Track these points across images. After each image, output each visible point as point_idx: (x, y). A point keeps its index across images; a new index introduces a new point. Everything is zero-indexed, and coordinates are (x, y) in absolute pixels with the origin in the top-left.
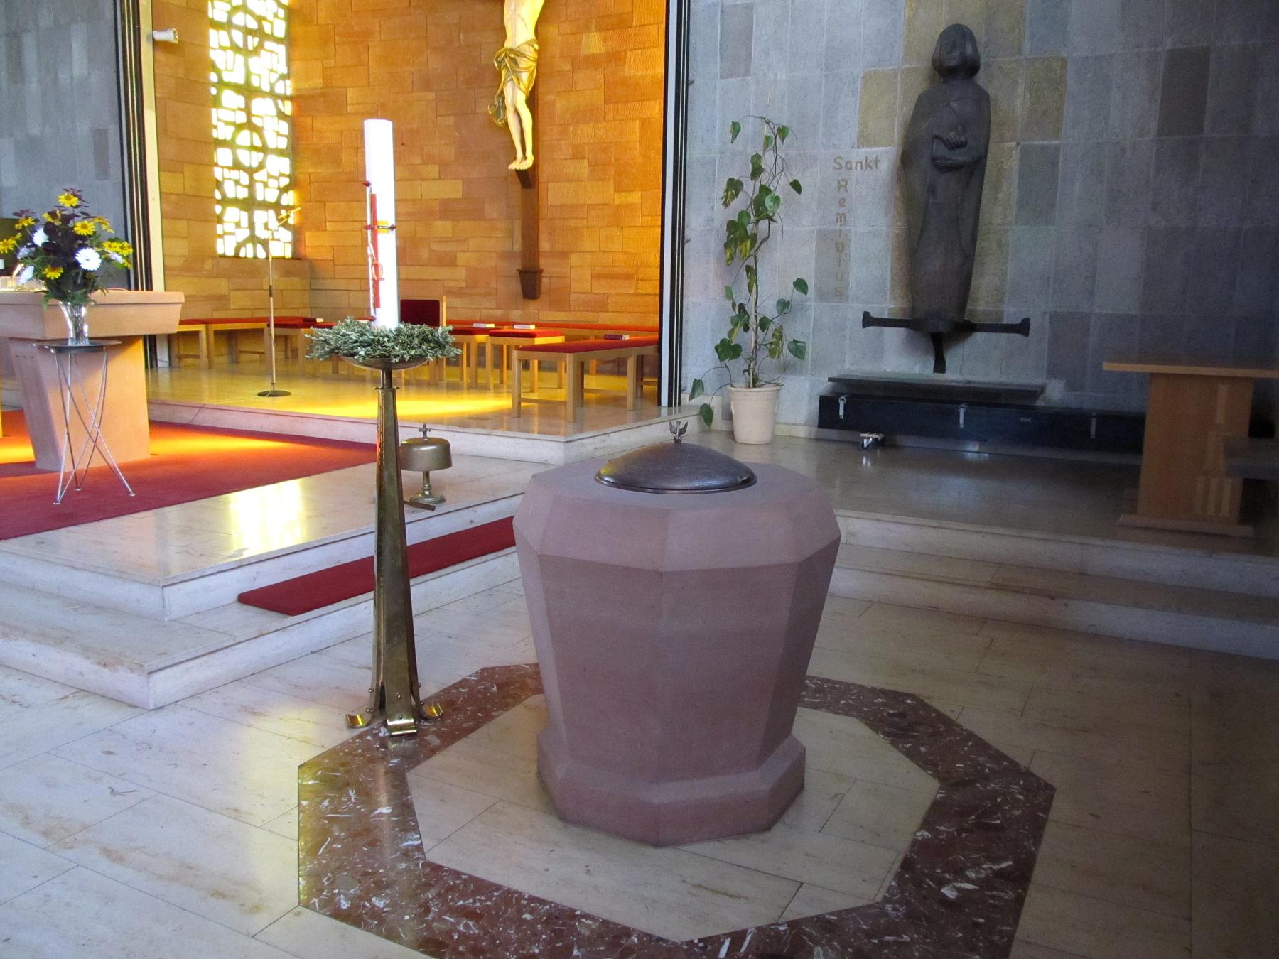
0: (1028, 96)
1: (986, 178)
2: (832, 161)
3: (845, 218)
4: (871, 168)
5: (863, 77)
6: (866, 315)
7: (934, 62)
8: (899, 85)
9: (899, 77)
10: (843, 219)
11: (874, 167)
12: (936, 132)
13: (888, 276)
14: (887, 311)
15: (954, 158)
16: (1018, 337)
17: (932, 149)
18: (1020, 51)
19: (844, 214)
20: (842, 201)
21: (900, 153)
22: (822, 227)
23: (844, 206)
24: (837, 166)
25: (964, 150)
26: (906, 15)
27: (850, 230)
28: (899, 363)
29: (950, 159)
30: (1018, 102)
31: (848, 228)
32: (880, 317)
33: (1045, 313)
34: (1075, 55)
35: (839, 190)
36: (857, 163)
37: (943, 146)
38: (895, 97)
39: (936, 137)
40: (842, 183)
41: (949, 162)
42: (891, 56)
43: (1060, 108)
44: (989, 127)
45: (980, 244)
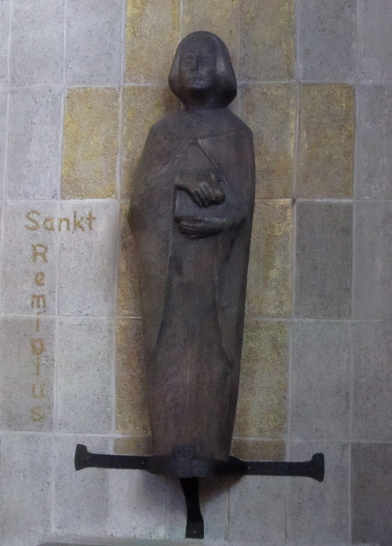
0: (305, 134)
1: (252, 248)
2: (23, 216)
3: (44, 302)
4: (83, 230)
5: (68, 97)
6: (81, 450)
7: (171, 82)
8: (120, 112)
9: (120, 99)
10: (41, 303)
11: (86, 226)
12: (178, 181)
13: (112, 390)
14: (111, 444)
15: (206, 219)
16: (309, 481)
17: (174, 205)
18: (290, 74)
19: (43, 296)
20: (40, 277)
21: (127, 207)
22: (10, 315)
23: (43, 284)
24: (31, 224)
25: (221, 207)
26: (129, 13)
27: (52, 322)
28: (134, 524)
29: (200, 221)
30: (292, 143)
31: (49, 317)
32: (101, 452)
33: (344, 446)
34: (365, 82)
35: (35, 259)
36: (61, 221)
37: (189, 201)
38: (116, 127)
39: (179, 188)
40: (40, 250)
41: (199, 225)
42: (108, 68)
43: (348, 154)
44: (254, 176)
45: (247, 345)
